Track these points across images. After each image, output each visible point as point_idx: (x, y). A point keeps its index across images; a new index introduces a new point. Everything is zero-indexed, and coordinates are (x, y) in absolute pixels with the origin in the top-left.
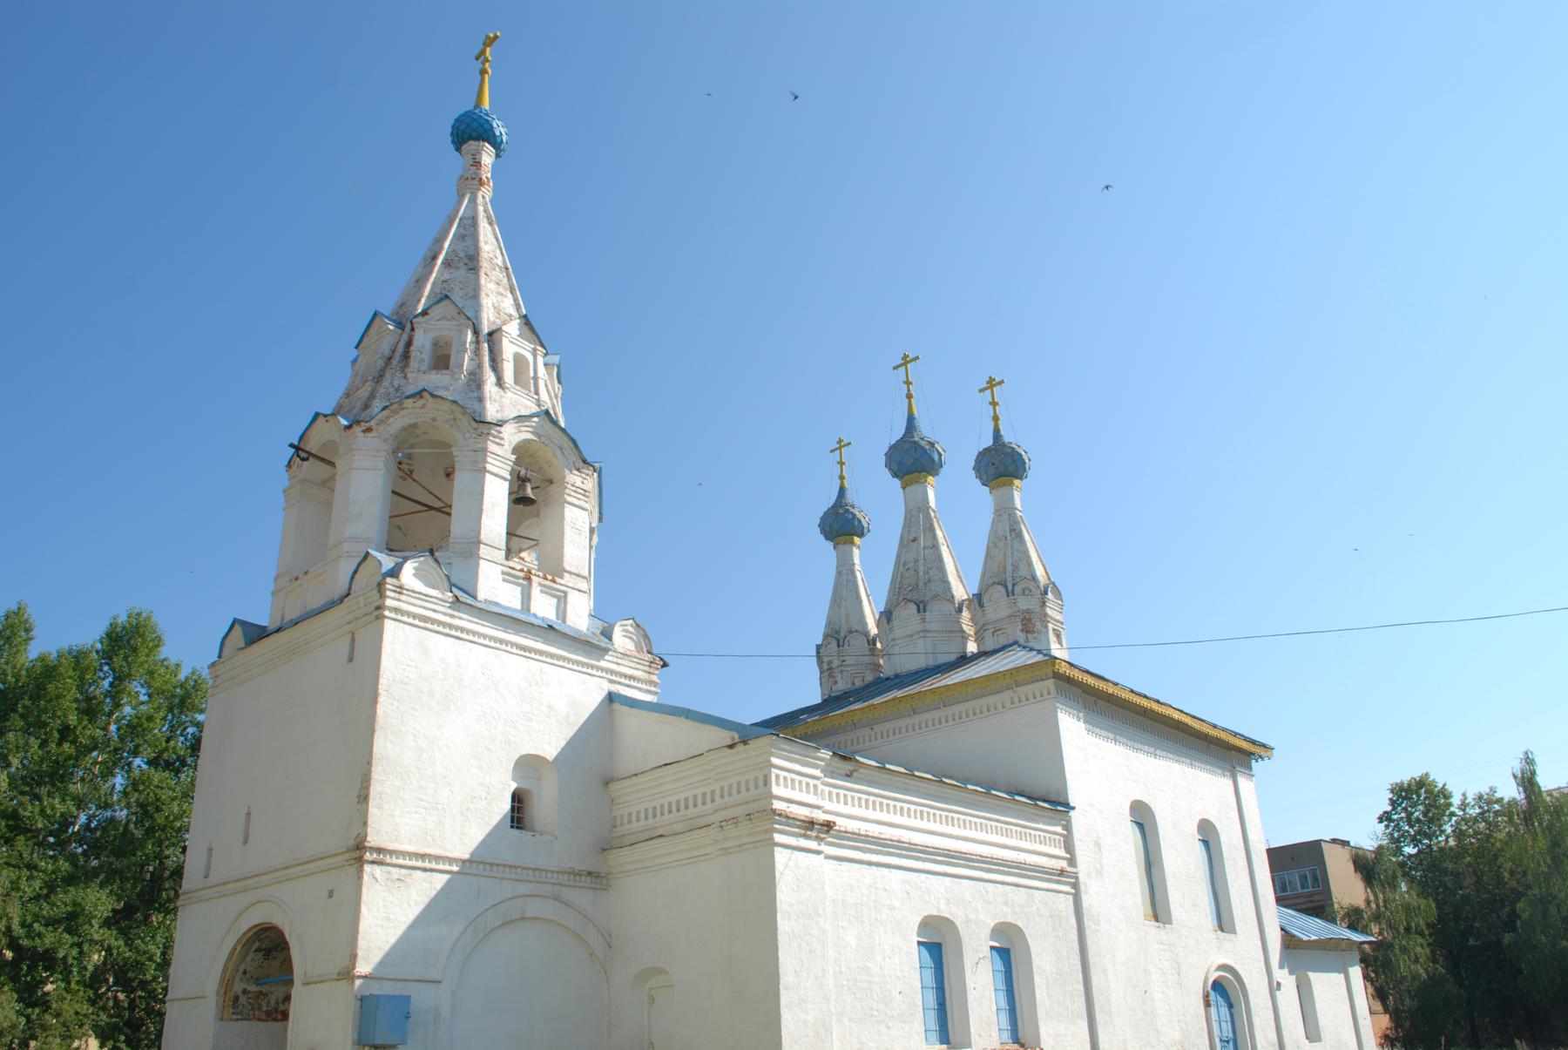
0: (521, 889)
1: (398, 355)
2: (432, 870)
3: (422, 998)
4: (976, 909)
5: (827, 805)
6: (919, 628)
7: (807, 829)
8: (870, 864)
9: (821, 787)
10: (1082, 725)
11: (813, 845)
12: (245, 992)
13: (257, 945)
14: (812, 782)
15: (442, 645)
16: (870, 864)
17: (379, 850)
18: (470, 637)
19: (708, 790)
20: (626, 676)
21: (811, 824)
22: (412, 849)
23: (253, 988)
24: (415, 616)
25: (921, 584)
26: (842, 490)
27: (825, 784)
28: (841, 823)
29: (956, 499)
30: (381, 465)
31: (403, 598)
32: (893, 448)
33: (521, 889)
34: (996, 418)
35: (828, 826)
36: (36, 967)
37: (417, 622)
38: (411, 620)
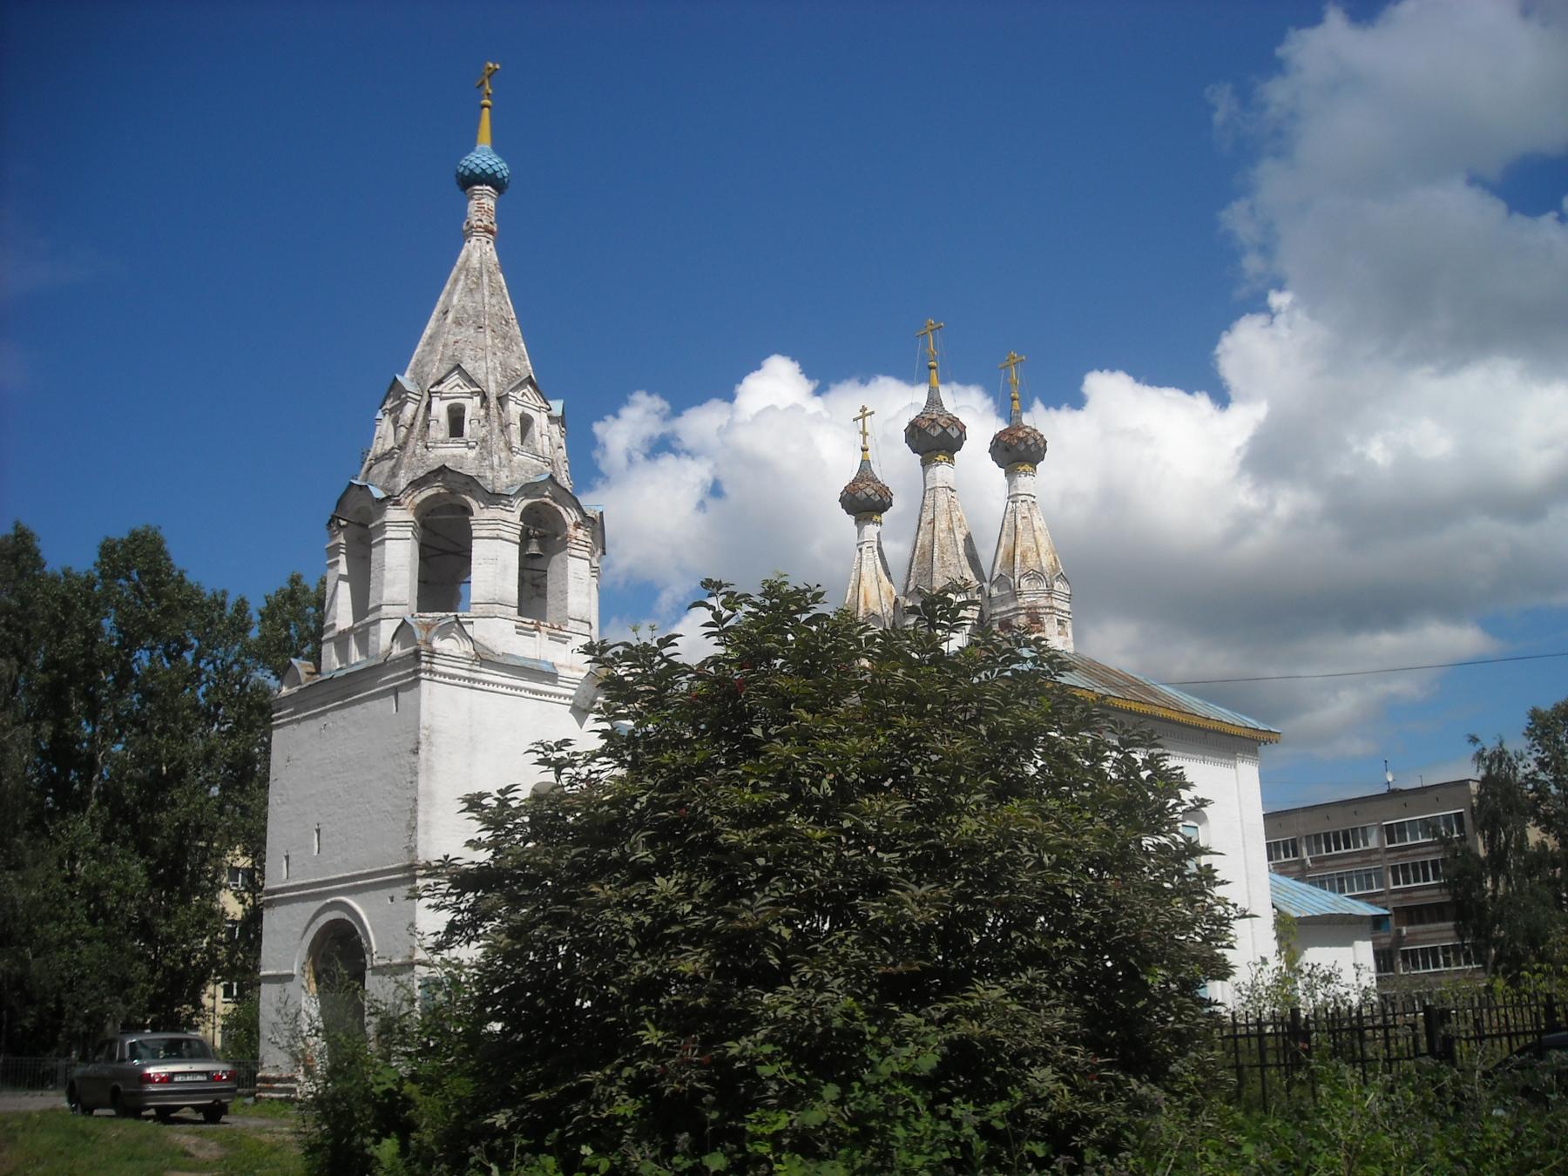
1: (420, 418)
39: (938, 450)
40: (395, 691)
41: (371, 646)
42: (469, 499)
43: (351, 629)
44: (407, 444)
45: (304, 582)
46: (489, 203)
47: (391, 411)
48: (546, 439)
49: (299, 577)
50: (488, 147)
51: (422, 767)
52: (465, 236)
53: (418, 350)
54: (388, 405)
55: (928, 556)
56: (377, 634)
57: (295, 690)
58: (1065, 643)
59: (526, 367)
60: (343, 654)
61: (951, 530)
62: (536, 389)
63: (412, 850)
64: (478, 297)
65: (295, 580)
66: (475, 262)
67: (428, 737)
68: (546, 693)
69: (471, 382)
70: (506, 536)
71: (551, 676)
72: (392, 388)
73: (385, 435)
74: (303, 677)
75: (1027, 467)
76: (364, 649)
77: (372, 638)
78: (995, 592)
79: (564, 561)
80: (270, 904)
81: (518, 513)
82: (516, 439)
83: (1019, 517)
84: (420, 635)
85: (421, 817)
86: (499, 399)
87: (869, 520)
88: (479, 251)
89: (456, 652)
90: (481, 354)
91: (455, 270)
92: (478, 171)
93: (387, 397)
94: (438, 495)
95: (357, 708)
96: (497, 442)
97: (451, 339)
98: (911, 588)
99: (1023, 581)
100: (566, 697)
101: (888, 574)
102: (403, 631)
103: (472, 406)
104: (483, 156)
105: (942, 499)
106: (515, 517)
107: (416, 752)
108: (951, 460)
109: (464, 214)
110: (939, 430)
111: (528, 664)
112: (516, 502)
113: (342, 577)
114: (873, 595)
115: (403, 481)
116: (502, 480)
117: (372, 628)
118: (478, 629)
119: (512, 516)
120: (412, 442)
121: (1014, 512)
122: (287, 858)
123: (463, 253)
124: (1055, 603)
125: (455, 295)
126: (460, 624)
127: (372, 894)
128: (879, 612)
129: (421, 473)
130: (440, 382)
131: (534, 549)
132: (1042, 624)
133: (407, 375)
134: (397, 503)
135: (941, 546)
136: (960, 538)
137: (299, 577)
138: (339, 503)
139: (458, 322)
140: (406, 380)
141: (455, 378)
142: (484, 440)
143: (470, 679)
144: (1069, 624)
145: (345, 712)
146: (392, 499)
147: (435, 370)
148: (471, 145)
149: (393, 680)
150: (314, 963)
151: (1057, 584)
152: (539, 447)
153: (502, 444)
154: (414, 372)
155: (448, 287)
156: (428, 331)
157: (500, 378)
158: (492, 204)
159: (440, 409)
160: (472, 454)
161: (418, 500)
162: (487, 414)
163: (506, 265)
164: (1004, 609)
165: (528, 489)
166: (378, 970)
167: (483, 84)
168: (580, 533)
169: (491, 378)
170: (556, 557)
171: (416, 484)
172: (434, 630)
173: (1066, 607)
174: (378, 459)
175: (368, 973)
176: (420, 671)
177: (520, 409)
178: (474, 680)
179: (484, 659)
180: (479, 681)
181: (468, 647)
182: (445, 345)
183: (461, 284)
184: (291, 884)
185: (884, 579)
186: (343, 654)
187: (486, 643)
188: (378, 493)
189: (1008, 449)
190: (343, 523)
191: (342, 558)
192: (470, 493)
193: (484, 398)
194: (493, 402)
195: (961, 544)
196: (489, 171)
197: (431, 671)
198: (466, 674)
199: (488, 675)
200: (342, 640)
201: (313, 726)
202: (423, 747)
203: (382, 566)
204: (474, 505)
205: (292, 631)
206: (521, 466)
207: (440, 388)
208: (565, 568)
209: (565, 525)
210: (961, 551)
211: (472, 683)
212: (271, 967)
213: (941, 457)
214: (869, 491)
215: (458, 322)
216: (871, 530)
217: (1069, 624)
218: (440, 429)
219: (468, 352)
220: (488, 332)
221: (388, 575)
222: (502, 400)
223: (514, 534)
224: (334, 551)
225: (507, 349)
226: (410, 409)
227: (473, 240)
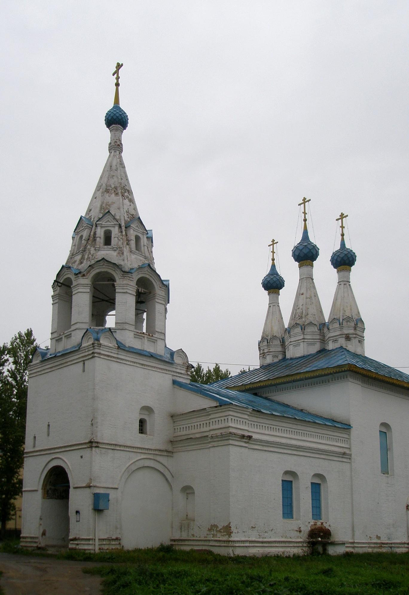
0: (143, 456)
2: (114, 449)
3: (113, 495)
4: (306, 469)
5: (250, 429)
6: (302, 337)
12: (50, 489)
15: (115, 366)
17: (97, 443)
18: (124, 362)
21: (243, 437)
22: (107, 442)
23: (53, 488)
24: (105, 355)
25: (303, 316)
26: (273, 266)
28: (255, 436)
29: (323, 270)
30: (89, 290)
32: (296, 248)
33: (143, 456)
34: (343, 235)
35: (250, 437)
38: (104, 357)
48: (146, 247)
70: (130, 292)
81: (135, 282)
103: (115, 231)
106: (134, 283)
110: (308, 250)
119: (133, 284)
126: (112, 332)
150: (206, 558)
152: (143, 251)
159: (100, 232)
175: (71, 490)
177: (136, 233)
193: (120, 227)
194: (123, 228)
199: (122, 355)
204: (117, 277)
211: (118, 360)
218: (100, 241)
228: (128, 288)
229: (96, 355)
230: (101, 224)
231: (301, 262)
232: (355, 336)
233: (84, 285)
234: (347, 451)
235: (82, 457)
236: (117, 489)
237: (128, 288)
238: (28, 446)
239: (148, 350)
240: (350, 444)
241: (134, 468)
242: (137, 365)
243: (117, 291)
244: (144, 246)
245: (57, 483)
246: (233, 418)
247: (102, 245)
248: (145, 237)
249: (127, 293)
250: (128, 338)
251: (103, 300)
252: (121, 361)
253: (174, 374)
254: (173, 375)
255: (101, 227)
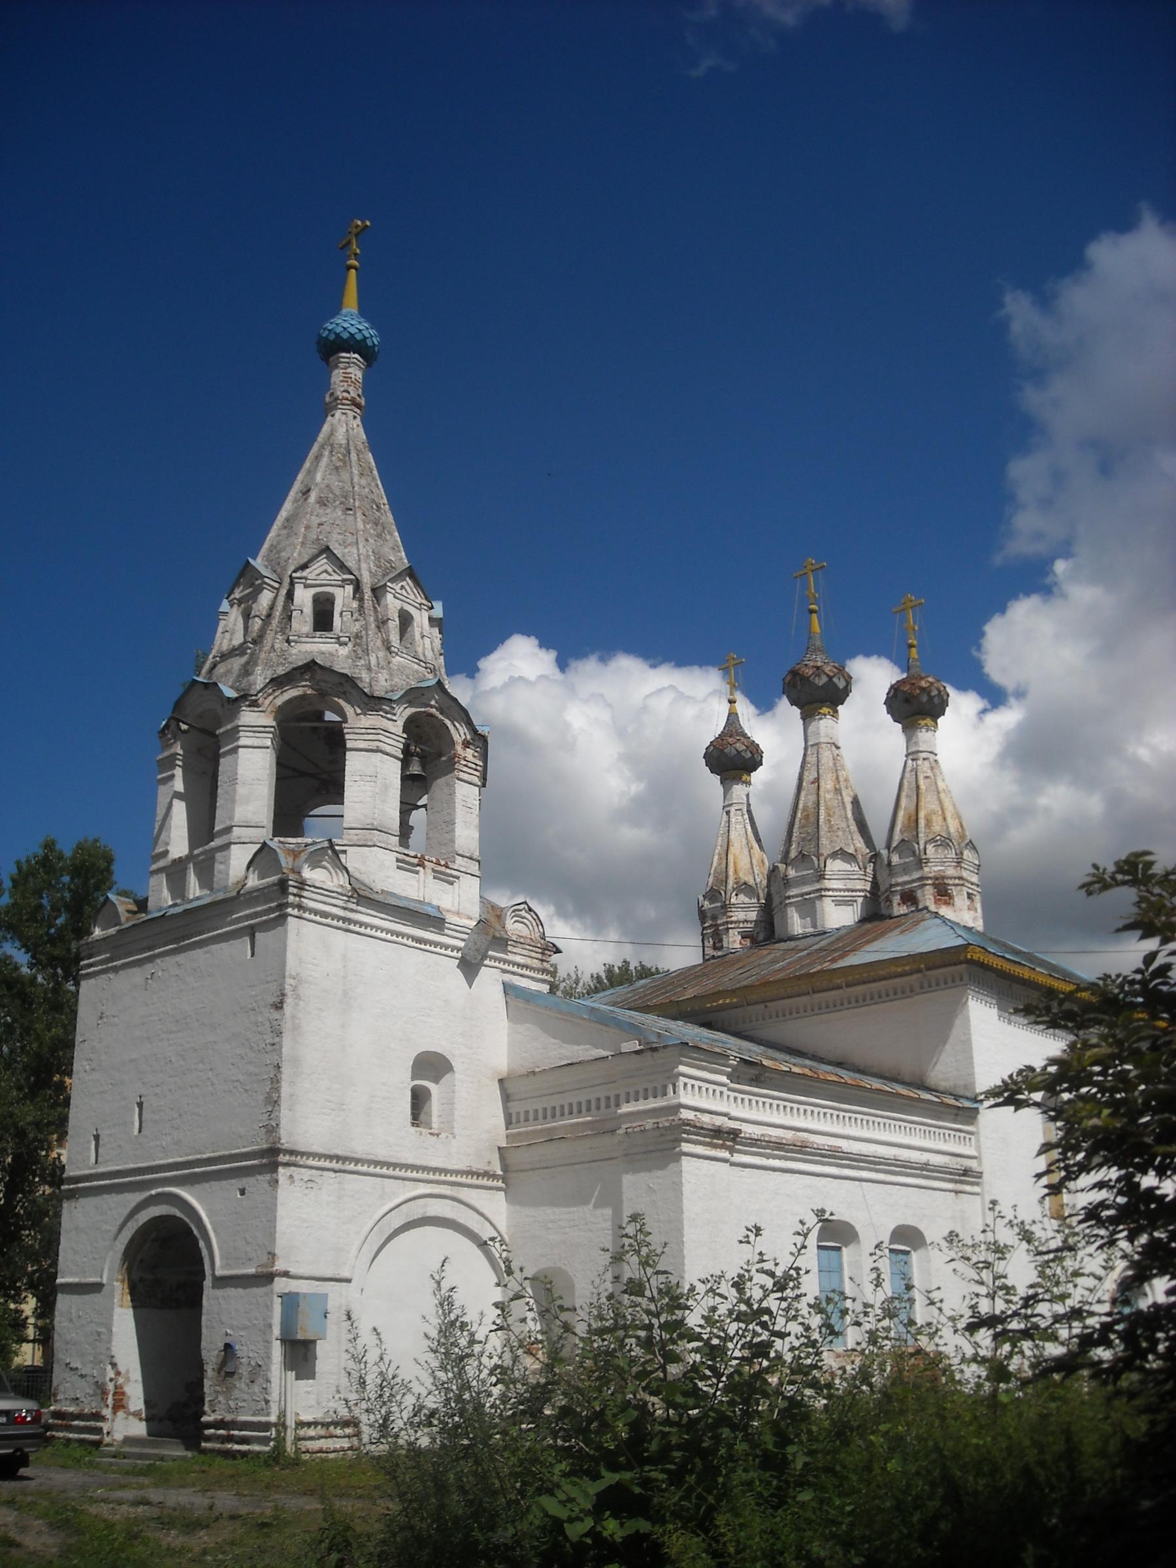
1: (278, 613)
7: (713, 1137)
8: (774, 1169)
9: (726, 1092)
10: (994, 1011)
11: (725, 1154)
13: (154, 1235)
14: (718, 1089)
15: (339, 939)
16: (774, 1169)
17: (292, 1152)
19: (612, 1094)
20: (519, 965)
21: (717, 1132)
27: (729, 1090)
28: (749, 1130)
30: (269, 743)
31: (305, 894)
35: (734, 1134)
36: (757, 1411)
37: (318, 918)
39: (823, 702)
40: (251, 931)
41: (217, 876)
42: (341, 702)
43: (190, 857)
44: (253, 642)
45: (58, 847)
46: (357, 373)
47: (240, 602)
48: (427, 641)
49: (53, 843)
50: (355, 311)
51: (287, 1026)
52: (327, 410)
53: (272, 534)
54: (237, 594)
55: (812, 819)
56: (226, 862)
57: (112, 931)
58: (975, 919)
59: (401, 560)
60: (178, 886)
61: (838, 791)
62: (417, 583)
63: (272, 1130)
64: (345, 476)
65: (49, 846)
66: (340, 437)
67: (295, 989)
68: (431, 943)
69: (342, 567)
70: (388, 749)
71: (436, 922)
72: (242, 574)
73: (231, 628)
74: (124, 915)
75: (929, 721)
76: (206, 879)
77: (218, 867)
78: (895, 859)
79: (451, 787)
80: (72, 1195)
81: (400, 723)
82: (394, 638)
83: (921, 777)
84: (285, 861)
85: (285, 1089)
86: (373, 590)
87: (738, 779)
88: (344, 426)
89: (329, 885)
90: (351, 539)
91: (315, 448)
92: (345, 335)
93: (237, 584)
94: (303, 697)
95: (198, 953)
96: (374, 640)
97: (315, 521)
98: (793, 854)
99: (930, 849)
100: (453, 948)
101: (759, 841)
102: (263, 857)
103: (343, 597)
104: (350, 320)
105: (826, 755)
106: (397, 727)
107: (279, 1006)
108: (835, 714)
109: (326, 385)
110: (824, 679)
111: (412, 906)
112: (399, 710)
113: (177, 795)
114: (744, 863)
115: (259, 678)
116: (381, 684)
117: (218, 856)
118: (353, 859)
119: (395, 724)
120: (269, 636)
121: (915, 771)
122: (97, 1138)
123: (326, 428)
124: (965, 874)
125: (318, 472)
127: (215, 1185)
128: (751, 882)
129: (281, 671)
130: (304, 567)
131: (415, 769)
132: (951, 897)
133: (259, 559)
134: (255, 704)
135: (827, 808)
136: (848, 800)
137: (53, 843)
138: (178, 705)
139: (322, 502)
140: (258, 563)
141: (322, 563)
142: (357, 636)
143: (345, 920)
144: (978, 898)
145: (181, 958)
146: (246, 698)
147: (297, 554)
148: (336, 308)
149: (248, 917)
150: (129, 1271)
151: (966, 852)
152: (420, 650)
153: (379, 643)
154: (267, 558)
155: (307, 465)
156: (283, 514)
157: (374, 568)
158: (359, 375)
159: (304, 597)
160: (344, 651)
161: (279, 702)
162: (361, 607)
163: (374, 443)
164: (906, 878)
165: (413, 695)
166: (222, 1282)
167: (349, 242)
168: (469, 753)
169: (364, 566)
170: (441, 782)
171: (278, 682)
172: (304, 856)
173: (975, 879)
174: (224, 657)
176: (287, 905)
177: (398, 604)
178: (350, 921)
179: (362, 896)
180: (356, 923)
181: (343, 879)
182: (307, 528)
183: (324, 461)
184: (101, 1169)
185: (756, 845)
186: (178, 886)
187: (362, 877)
188: (230, 693)
189: (908, 699)
190: (184, 727)
191: (178, 772)
192: (344, 695)
194: (368, 594)
195: (849, 807)
196: (359, 337)
197: (300, 907)
198: (341, 913)
199: (366, 916)
200: (176, 872)
201: (136, 976)
202: (289, 1001)
203: (234, 780)
205: (45, 902)
206: (401, 669)
207: (305, 573)
208: (452, 794)
209: (452, 743)
210: (850, 815)
211: (347, 925)
212: (71, 1274)
213: (825, 710)
214: (740, 747)
215: (322, 502)
216: (738, 790)
217: (978, 898)
218: (303, 622)
219: (335, 536)
220: (359, 514)
221: (241, 790)
222: (378, 592)
223: (395, 746)
224: (169, 763)
225: (379, 536)
226: (266, 597)
227: (338, 413)
228: (381, 737)
229: (289, 910)
230: (306, 579)
231: (807, 707)
232: (957, 881)
233: (255, 729)
234: (973, 1164)
235: (243, 1192)
236: (349, 1281)
237: (381, 737)
238: (75, 1155)
239: (435, 903)
240: (978, 1148)
241: (397, 1220)
242: (405, 941)
243: (349, 745)
244: (423, 637)
245: (168, 1270)
246: (690, 1082)
247: (307, 627)
248: (425, 615)
249: (378, 750)
250: (379, 867)
251: (303, 774)
252: (362, 930)
253: (506, 967)
254: (504, 971)
255: (306, 586)
